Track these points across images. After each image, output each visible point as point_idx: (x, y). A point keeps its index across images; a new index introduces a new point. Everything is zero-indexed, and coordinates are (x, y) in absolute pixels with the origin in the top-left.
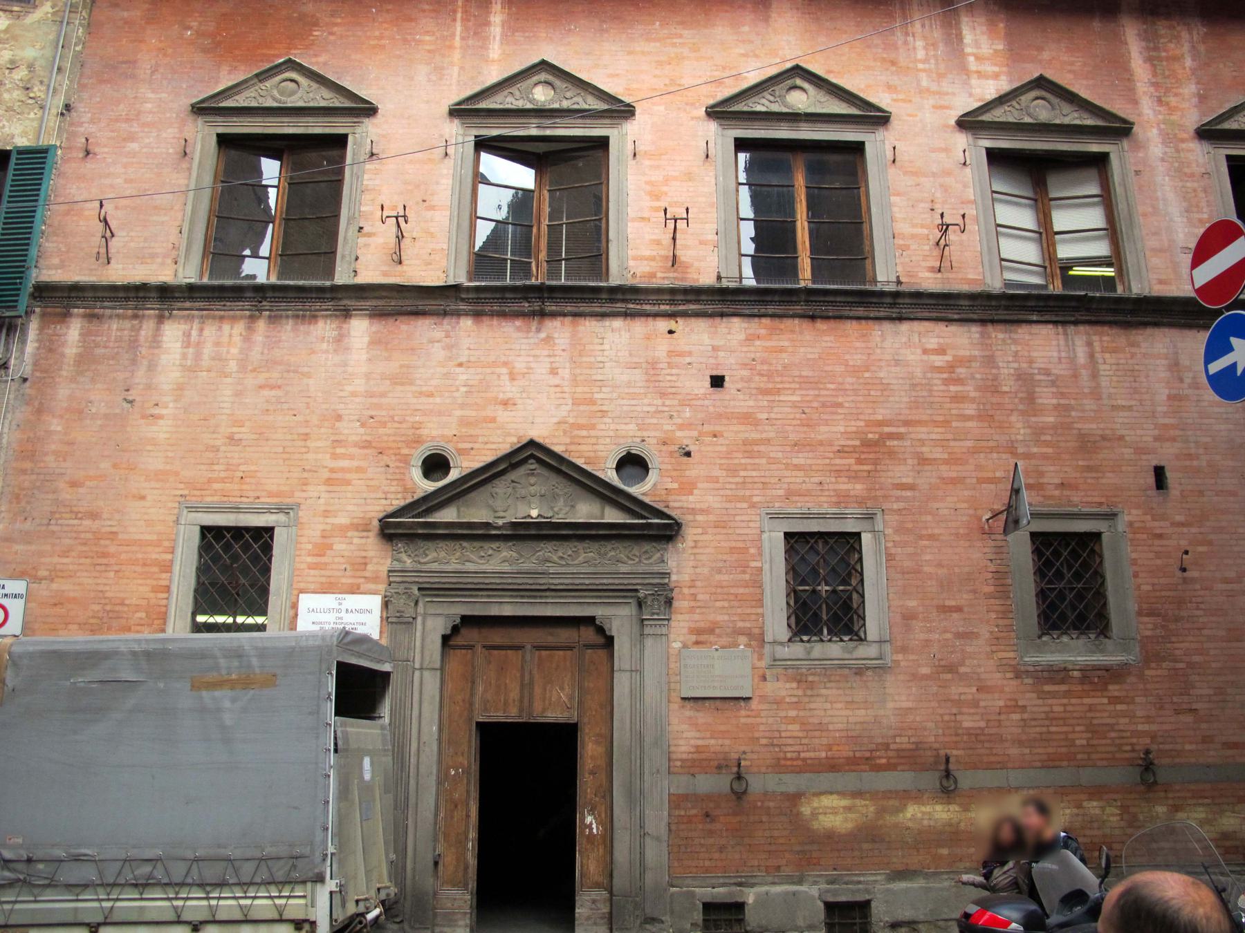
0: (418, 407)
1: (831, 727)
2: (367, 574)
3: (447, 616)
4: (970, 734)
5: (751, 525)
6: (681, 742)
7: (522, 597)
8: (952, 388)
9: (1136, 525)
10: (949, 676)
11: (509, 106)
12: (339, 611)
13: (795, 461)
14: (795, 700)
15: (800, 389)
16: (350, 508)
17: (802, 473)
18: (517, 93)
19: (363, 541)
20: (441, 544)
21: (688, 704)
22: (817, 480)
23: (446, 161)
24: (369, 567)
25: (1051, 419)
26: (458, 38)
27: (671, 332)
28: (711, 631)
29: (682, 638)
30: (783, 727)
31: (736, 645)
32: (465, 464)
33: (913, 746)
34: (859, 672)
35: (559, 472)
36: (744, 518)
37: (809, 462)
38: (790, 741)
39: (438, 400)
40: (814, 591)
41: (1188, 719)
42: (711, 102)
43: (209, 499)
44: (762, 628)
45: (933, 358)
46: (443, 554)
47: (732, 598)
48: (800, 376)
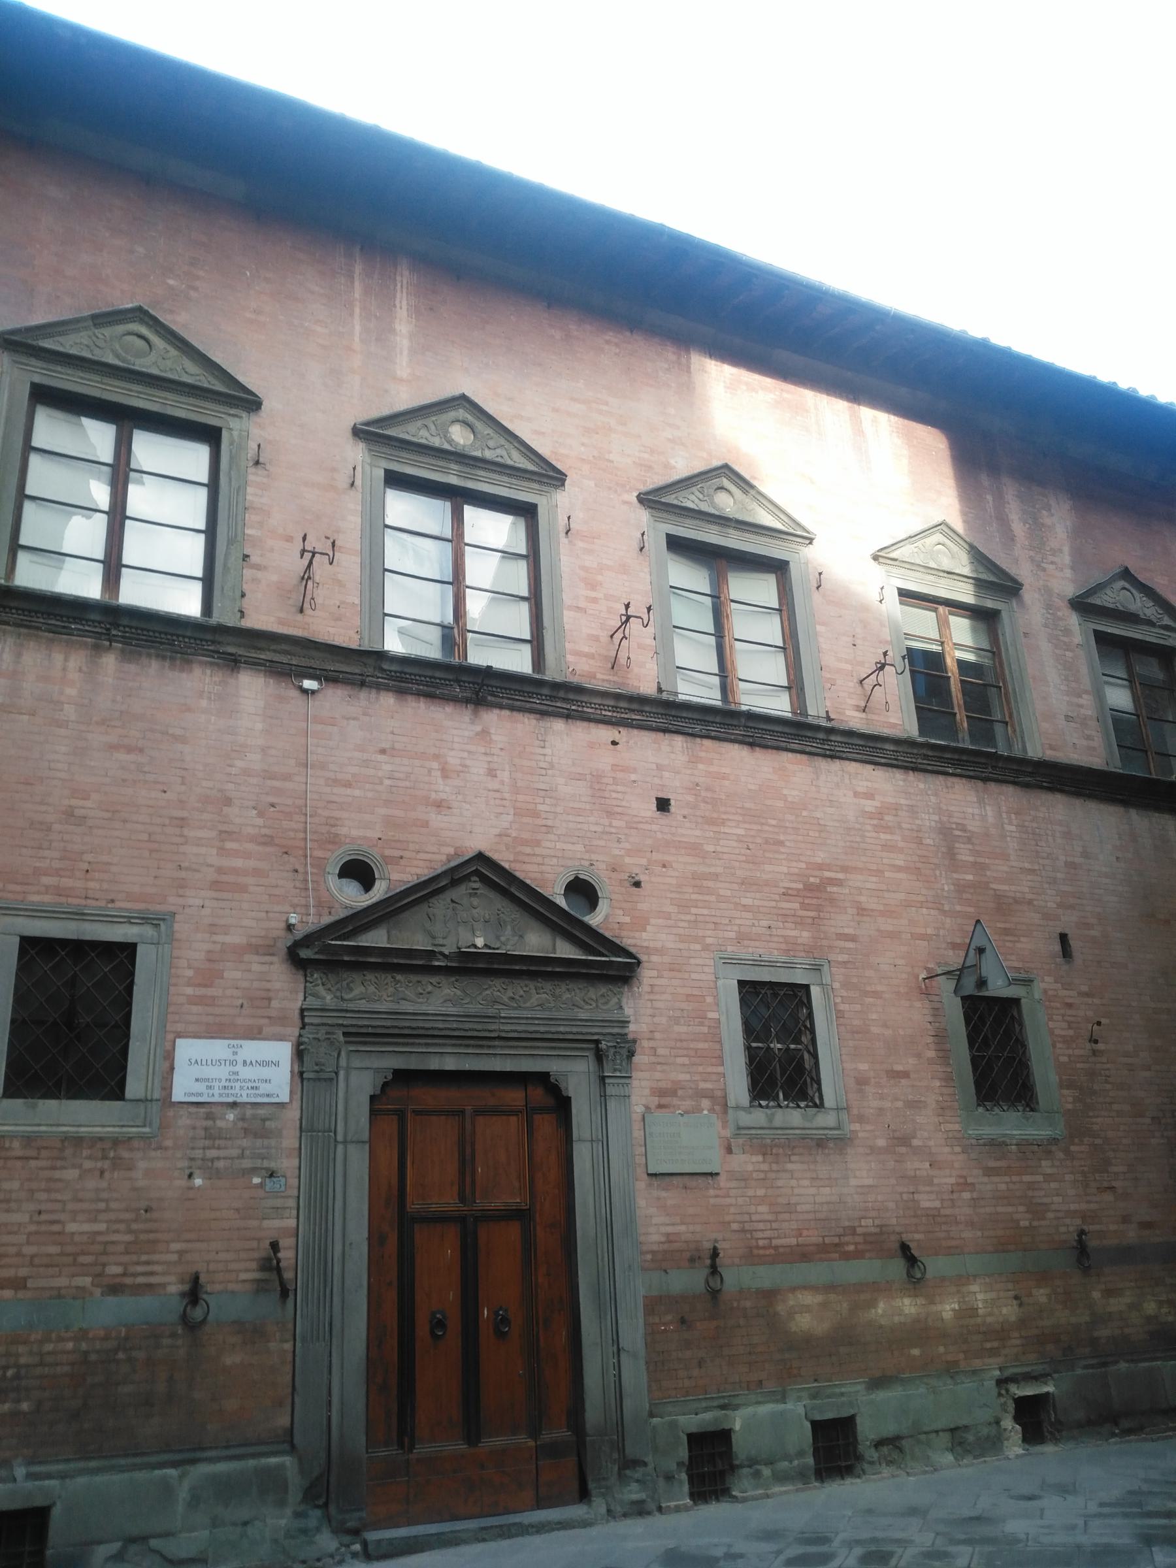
0: (334, 798)
1: (799, 1208)
2: (274, 1013)
3: (377, 1070)
4: (928, 1215)
5: (706, 969)
6: (652, 1230)
7: (467, 1046)
8: (882, 836)
9: (1050, 993)
10: (903, 1150)
11: (423, 441)
12: (233, 1063)
13: (744, 901)
14: (762, 1175)
15: (745, 822)
16: (246, 922)
17: (749, 916)
18: (432, 427)
19: (265, 968)
20: (370, 976)
21: (655, 1182)
22: (765, 923)
23: (352, 493)
24: (275, 1004)
25: (970, 877)
26: (357, 339)
27: (614, 743)
28: (673, 1092)
29: (644, 1101)
30: (752, 1209)
31: (698, 1110)
32: (395, 876)
33: (877, 1230)
34: (821, 1143)
35: (505, 893)
36: (699, 961)
37: (757, 903)
38: (761, 1226)
39: (357, 793)
40: (769, 1048)
41: (1108, 1197)
42: (644, 489)
43: (35, 898)
44: (725, 1090)
45: (863, 802)
46: (372, 989)
47: (692, 1053)
48: (742, 808)
